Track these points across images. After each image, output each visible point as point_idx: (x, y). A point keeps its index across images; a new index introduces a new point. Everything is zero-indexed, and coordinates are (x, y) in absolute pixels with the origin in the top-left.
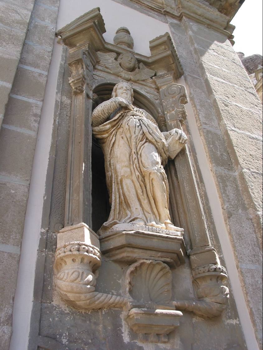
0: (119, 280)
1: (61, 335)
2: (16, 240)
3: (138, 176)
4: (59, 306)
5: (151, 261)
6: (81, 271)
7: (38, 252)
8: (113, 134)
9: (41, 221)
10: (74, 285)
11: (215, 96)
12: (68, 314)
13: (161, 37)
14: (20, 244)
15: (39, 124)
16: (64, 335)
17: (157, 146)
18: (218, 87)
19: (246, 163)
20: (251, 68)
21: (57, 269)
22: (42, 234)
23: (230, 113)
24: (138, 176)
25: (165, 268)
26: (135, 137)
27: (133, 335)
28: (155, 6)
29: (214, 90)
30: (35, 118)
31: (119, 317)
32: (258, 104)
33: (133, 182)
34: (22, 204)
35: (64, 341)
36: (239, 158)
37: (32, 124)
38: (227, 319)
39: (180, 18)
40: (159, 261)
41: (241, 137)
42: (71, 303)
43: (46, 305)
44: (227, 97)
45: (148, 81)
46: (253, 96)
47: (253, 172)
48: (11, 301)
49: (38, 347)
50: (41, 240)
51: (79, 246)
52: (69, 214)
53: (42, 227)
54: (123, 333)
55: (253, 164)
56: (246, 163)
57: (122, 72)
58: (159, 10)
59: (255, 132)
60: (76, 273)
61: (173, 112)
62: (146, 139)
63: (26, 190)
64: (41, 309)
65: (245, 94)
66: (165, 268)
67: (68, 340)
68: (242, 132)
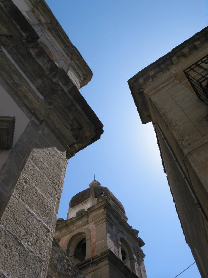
11: (22, 172)
13: (9, 117)
18: (29, 169)
19: (7, 222)
20: (98, 194)
23: (24, 188)
28: (30, 107)
29: (25, 169)
32: (54, 197)
36: (4, 215)
39: (41, 122)
41: (19, 205)
44: (32, 178)
46: (54, 190)
47: (7, 230)
55: (12, 226)
56: (7, 222)
58: (31, 110)
59: (35, 210)
65: (49, 186)
68: (24, 203)
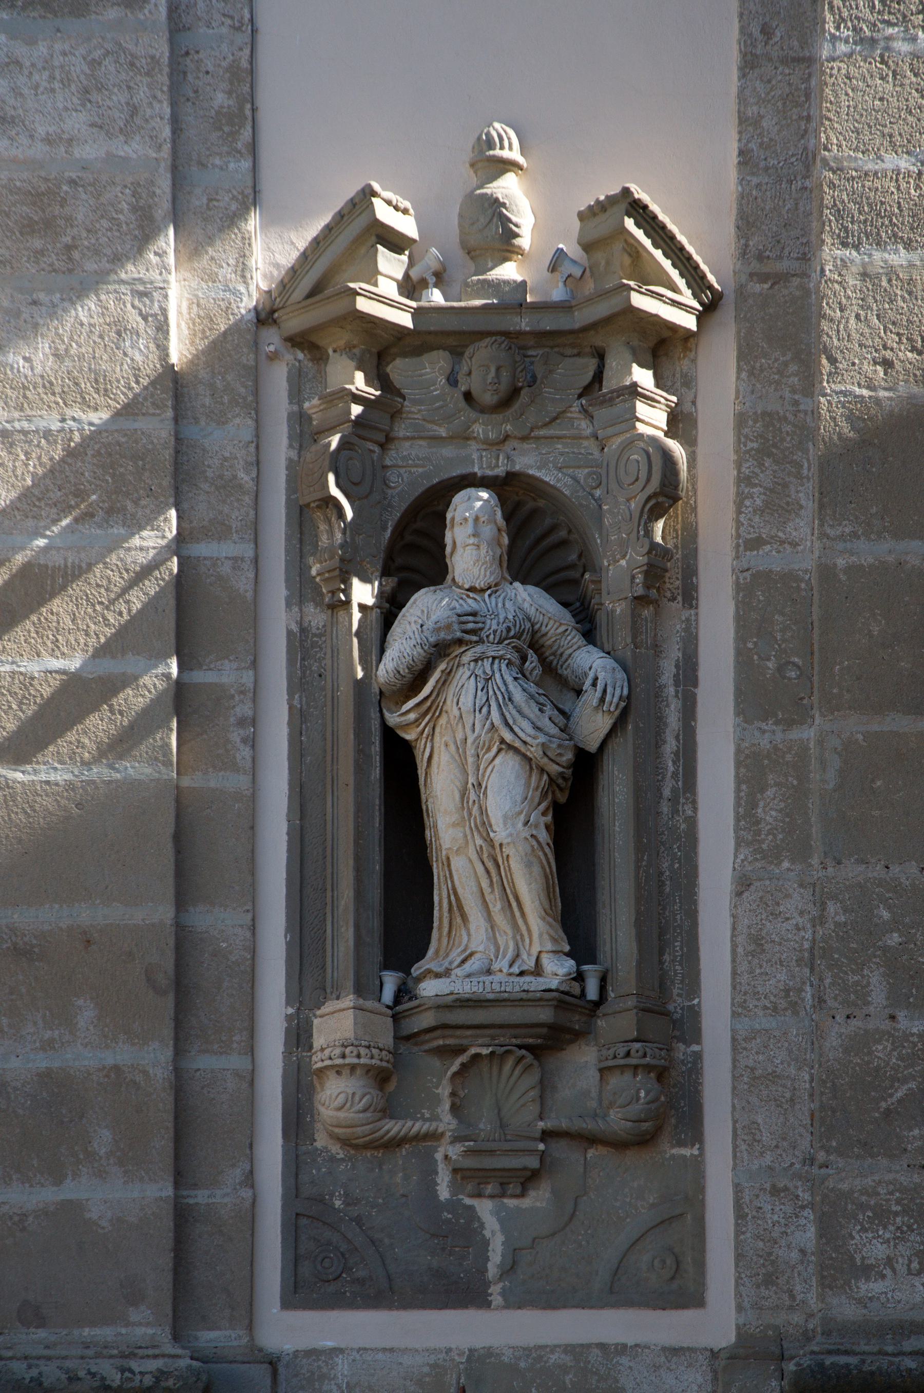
0: (437, 1089)
1: (332, 1195)
2: (243, 1044)
3: (481, 847)
4: (326, 1148)
5: (491, 1049)
6: (350, 1091)
7: (284, 1057)
8: (424, 735)
9: (283, 990)
10: (342, 1115)
12: (342, 1159)
14: (251, 1050)
15: (253, 747)
16: (337, 1194)
17: (528, 754)
21: (320, 1083)
22: (289, 1018)
24: (481, 847)
25: (523, 1057)
26: (475, 741)
27: (455, 1187)
30: (241, 732)
31: (433, 1158)
33: (470, 861)
34: (242, 968)
35: (338, 1203)
37: (238, 755)
38: (673, 1147)
40: (509, 1048)
42: (345, 1142)
43: (304, 1148)
45: (571, 412)
48: (248, 1152)
49: (297, 1214)
50: (288, 1031)
51: (343, 1049)
52: (333, 972)
53: (288, 1003)
54: (438, 1184)
57: (475, 422)
60: (342, 1096)
61: (623, 563)
62: (501, 743)
63: (248, 934)
64: (297, 1156)
66: (523, 1057)
67: (344, 1201)
